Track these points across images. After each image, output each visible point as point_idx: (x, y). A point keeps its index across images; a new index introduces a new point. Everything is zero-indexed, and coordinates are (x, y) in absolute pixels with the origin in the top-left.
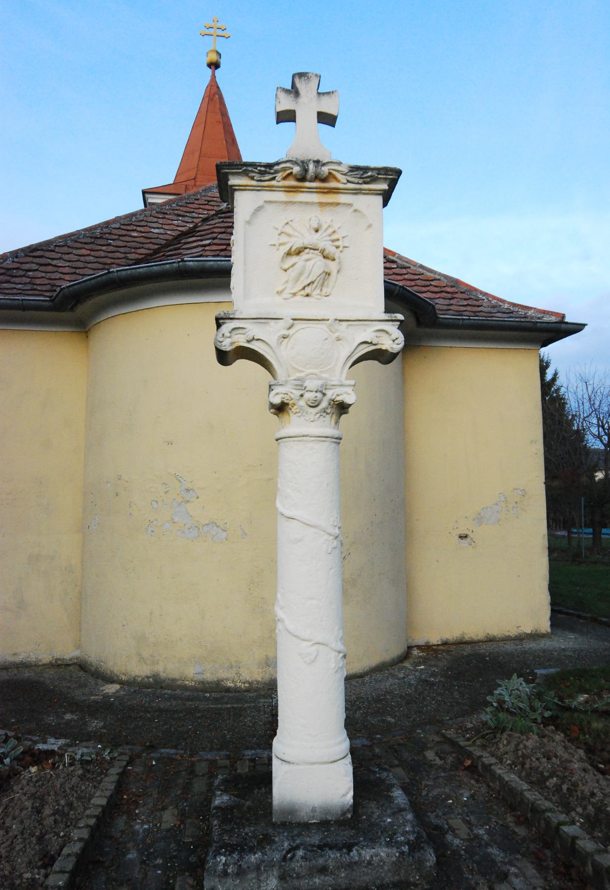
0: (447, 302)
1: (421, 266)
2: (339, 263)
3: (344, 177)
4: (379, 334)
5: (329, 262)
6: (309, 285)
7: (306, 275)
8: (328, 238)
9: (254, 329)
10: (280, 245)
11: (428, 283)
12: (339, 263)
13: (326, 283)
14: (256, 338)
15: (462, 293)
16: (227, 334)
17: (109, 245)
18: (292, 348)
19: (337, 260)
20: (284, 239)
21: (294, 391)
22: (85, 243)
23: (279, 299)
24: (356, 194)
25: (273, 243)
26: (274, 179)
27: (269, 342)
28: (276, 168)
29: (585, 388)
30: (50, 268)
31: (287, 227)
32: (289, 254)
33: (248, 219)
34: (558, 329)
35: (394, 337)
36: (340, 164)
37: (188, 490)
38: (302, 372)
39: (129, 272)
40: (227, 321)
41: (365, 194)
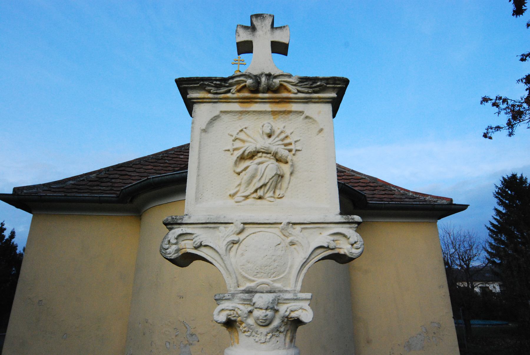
0: (371, 192)
1: (353, 171)
2: (292, 166)
3: (294, 87)
4: (335, 237)
5: (282, 165)
6: (261, 187)
7: (258, 177)
8: (281, 142)
9: (202, 235)
10: (234, 150)
11: (358, 181)
12: (292, 166)
13: (279, 186)
14: (203, 244)
15: (380, 186)
16: (173, 241)
17: (166, 163)
18: (242, 255)
19: (290, 163)
20: (238, 144)
21: (241, 307)
22: (152, 162)
23: (231, 202)
24: (307, 103)
25: (227, 149)
26: (229, 91)
27: (217, 249)
28: (231, 81)
29: (448, 237)
30: (126, 177)
31: (241, 133)
32: (242, 158)
33: (204, 127)
34: (449, 208)
35: (352, 240)
36: (290, 76)
37: (192, 335)
38: (253, 281)
39: (160, 178)
40: (175, 226)
41: (315, 102)
